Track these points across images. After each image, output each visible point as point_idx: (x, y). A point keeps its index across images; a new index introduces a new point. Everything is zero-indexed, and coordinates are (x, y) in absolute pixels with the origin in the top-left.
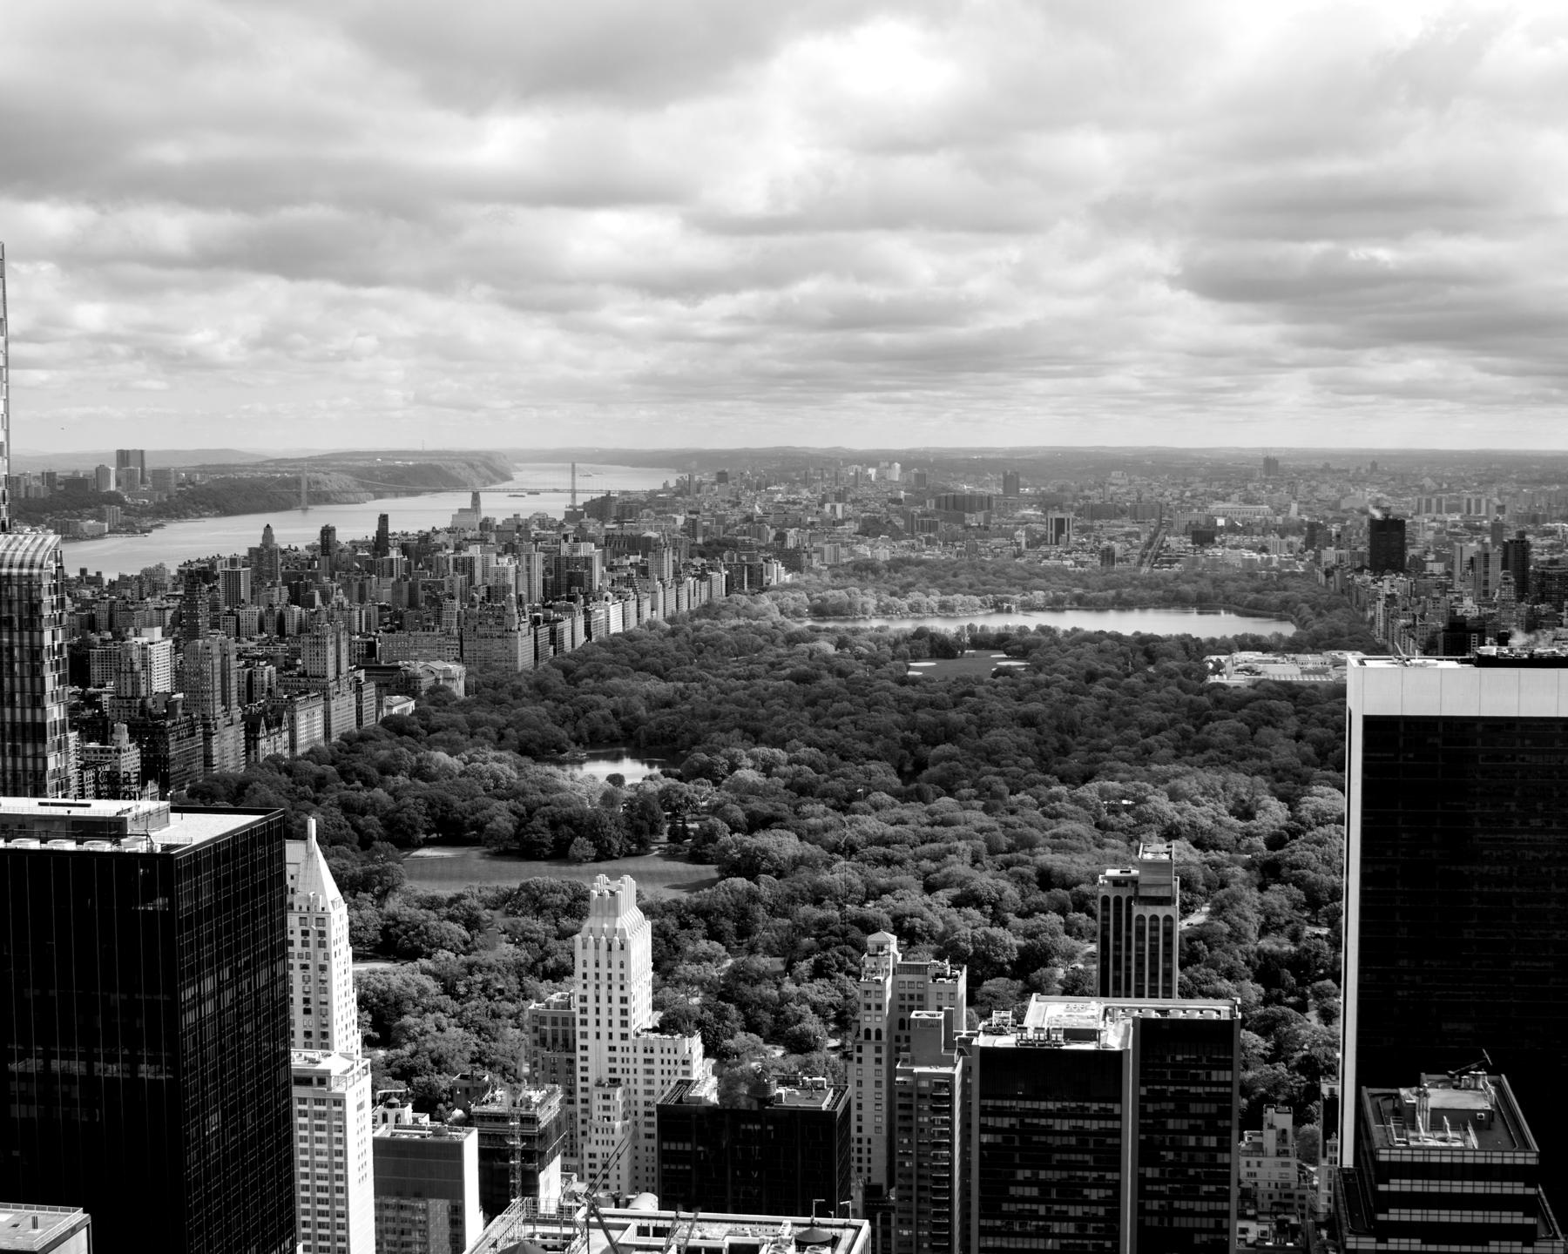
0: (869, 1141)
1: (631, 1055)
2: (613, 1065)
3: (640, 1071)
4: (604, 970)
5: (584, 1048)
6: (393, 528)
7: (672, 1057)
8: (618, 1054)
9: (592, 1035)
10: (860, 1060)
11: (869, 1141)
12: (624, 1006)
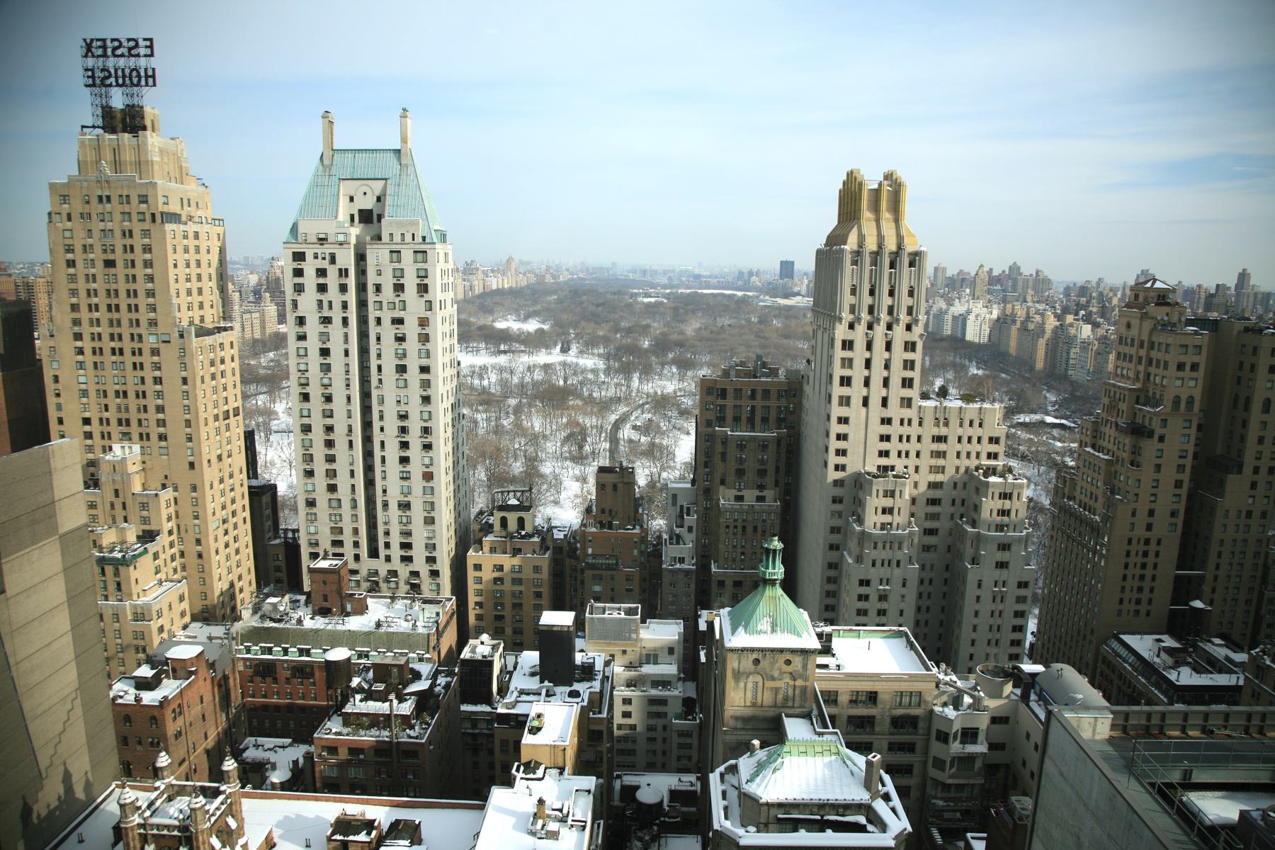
0: (1159, 543)
5: (843, 420)
7: (975, 432)
8: (894, 430)
9: (856, 401)
10: (1161, 439)
11: (1159, 543)
12: (321, 281)
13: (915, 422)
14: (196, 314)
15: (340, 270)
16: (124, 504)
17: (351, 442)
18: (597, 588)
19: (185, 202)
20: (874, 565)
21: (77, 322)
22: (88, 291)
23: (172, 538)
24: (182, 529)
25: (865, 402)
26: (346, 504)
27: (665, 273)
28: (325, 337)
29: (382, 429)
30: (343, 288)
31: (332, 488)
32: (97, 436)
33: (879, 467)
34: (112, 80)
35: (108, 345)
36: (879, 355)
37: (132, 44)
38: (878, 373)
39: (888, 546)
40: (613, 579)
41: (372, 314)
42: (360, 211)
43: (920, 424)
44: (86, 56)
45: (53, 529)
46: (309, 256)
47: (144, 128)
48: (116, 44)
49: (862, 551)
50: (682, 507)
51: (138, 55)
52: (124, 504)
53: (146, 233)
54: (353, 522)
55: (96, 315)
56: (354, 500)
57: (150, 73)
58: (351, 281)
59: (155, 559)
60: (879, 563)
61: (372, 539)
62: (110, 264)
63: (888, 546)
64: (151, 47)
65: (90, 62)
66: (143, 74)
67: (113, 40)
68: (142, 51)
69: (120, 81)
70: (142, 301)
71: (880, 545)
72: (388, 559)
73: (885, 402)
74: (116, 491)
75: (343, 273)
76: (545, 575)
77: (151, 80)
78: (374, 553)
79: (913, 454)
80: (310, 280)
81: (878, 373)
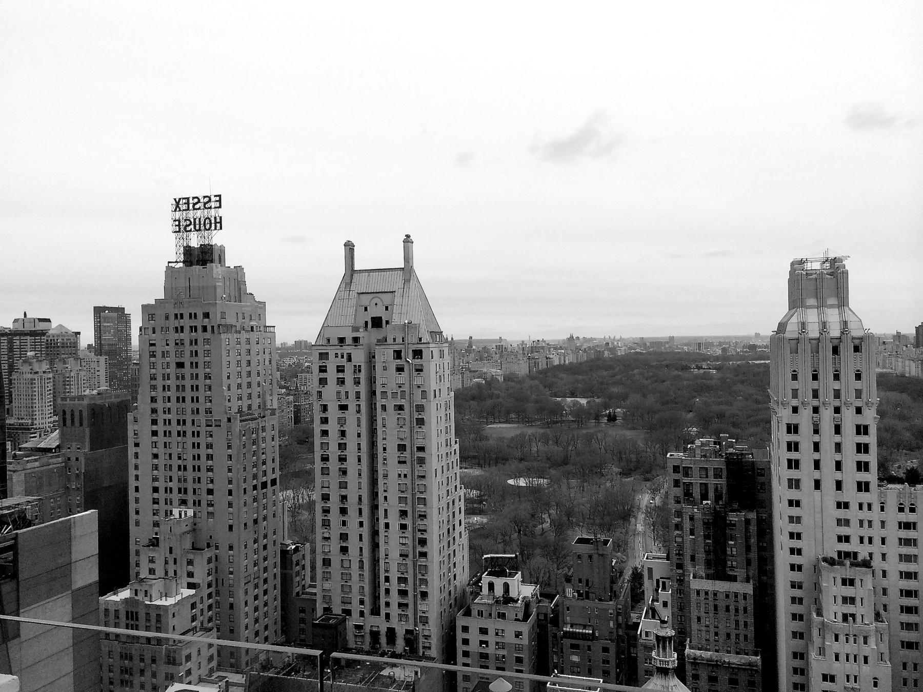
1: (875, 515)
2: (844, 531)
3: (892, 541)
4: (828, 385)
6: (28, 316)
8: (853, 514)
9: (807, 484)
12: (341, 375)
13: (876, 507)
14: (245, 403)
15: (355, 366)
16: (175, 560)
17: (360, 510)
18: (575, 658)
19: (240, 316)
20: (837, 659)
21: (154, 411)
22: (164, 386)
23: (210, 590)
24: (220, 582)
25: (817, 485)
26: (355, 566)
27: (720, 344)
28: (342, 421)
29: (386, 498)
30: (357, 382)
31: (344, 550)
32: (162, 502)
33: (839, 553)
34: (192, 227)
35: (175, 428)
36: (828, 438)
37: (206, 200)
38: (828, 457)
39: (851, 639)
40: (589, 649)
41: (380, 401)
42: (372, 318)
43: (882, 509)
44: (175, 210)
45: (67, 586)
46: (331, 356)
47: (212, 261)
48: (196, 200)
49: (824, 643)
50: (658, 581)
51: (210, 208)
52: (175, 560)
53: (207, 341)
54: (359, 584)
55: (169, 405)
56: (361, 562)
57: (218, 220)
58: (363, 376)
59: (192, 609)
60: (842, 657)
61: (376, 598)
62: (180, 365)
63: (851, 639)
64: (220, 201)
65: (178, 215)
66: (213, 221)
67: (194, 198)
68: (213, 204)
69: (197, 227)
70: (201, 394)
71: (842, 638)
72: (388, 616)
73: (839, 485)
74: (171, 549)
75: (357, 369)
76: (525, 640)
77: (218, 225)
78: (375, 611)
79: (877, 540)
80: (332, 375)
81: (828, 457)
